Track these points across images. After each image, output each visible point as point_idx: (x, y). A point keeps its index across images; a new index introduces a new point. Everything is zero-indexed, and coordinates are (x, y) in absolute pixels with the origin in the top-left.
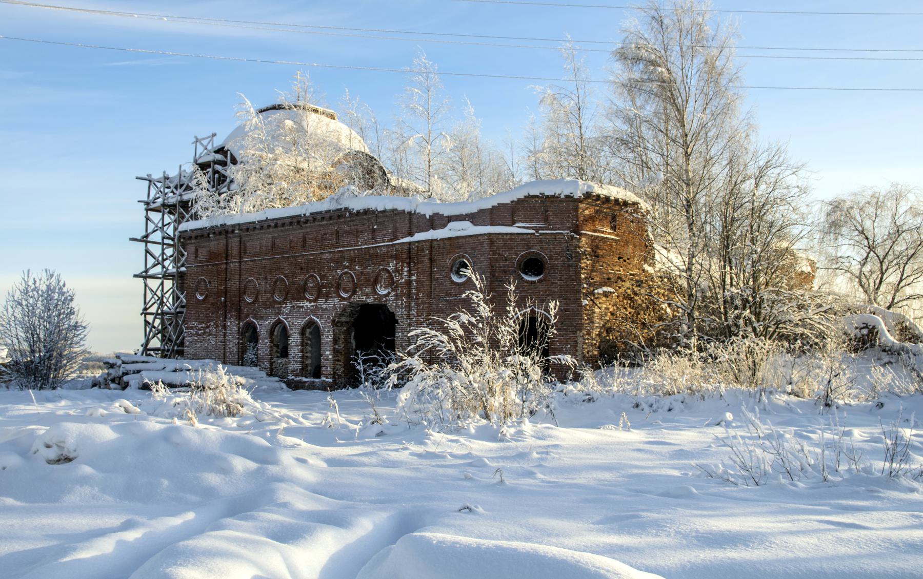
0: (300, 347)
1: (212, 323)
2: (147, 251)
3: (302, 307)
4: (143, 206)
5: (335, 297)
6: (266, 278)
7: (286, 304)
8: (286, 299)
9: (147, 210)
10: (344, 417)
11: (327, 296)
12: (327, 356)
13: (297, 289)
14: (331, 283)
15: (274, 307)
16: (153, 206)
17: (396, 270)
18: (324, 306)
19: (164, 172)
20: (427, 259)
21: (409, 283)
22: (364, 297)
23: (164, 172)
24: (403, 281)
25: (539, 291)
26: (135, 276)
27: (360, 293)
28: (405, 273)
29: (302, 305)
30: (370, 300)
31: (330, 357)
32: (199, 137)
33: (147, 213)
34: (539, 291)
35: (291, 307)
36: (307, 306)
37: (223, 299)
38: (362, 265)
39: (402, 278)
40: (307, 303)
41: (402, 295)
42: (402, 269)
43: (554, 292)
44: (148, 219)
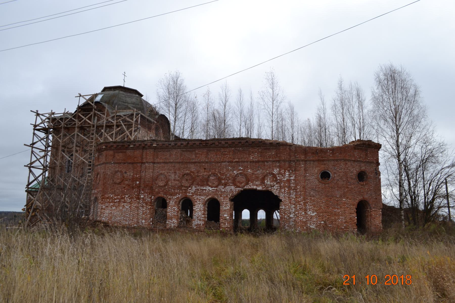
0: (203, 212)
1: (127, 196)
2: (32, 152)
3: (205, 190)
4: (32, 127)
5: (231, 185)
6: (175, 173)
7: (192, 187)
8: (192, 184)
9: (34, 129)
10: (166, 248)
11: (225, 185)
12: (225, 217)
13: (201, 180)
14: (228, 178)
15: (181, 189)
16: (38, 128)
17: (279, 173)
18: (223, 190)
19: (52, 111)
20: (302, 169)
21: (289, 181)
22: (255, 186)
23: (52, 111)
24: (285, 179)
25: (366, 189)
26: (25, 166)
27: (252, 184)
28: (287, 176)
29: (204, 188)
30: (260, 188)
31: (228, 218)
32: (82, 94)
33: (34, 131)
34: (366, 189)
35: (196, 189)
36: (209, 189)
37: (138, 182)
38: (253, 170)
39: (285, 178)
40: (210, 188)
41: (284, 187)
42: (285, 173)
43: (371, 190)
44: (34, 134)
